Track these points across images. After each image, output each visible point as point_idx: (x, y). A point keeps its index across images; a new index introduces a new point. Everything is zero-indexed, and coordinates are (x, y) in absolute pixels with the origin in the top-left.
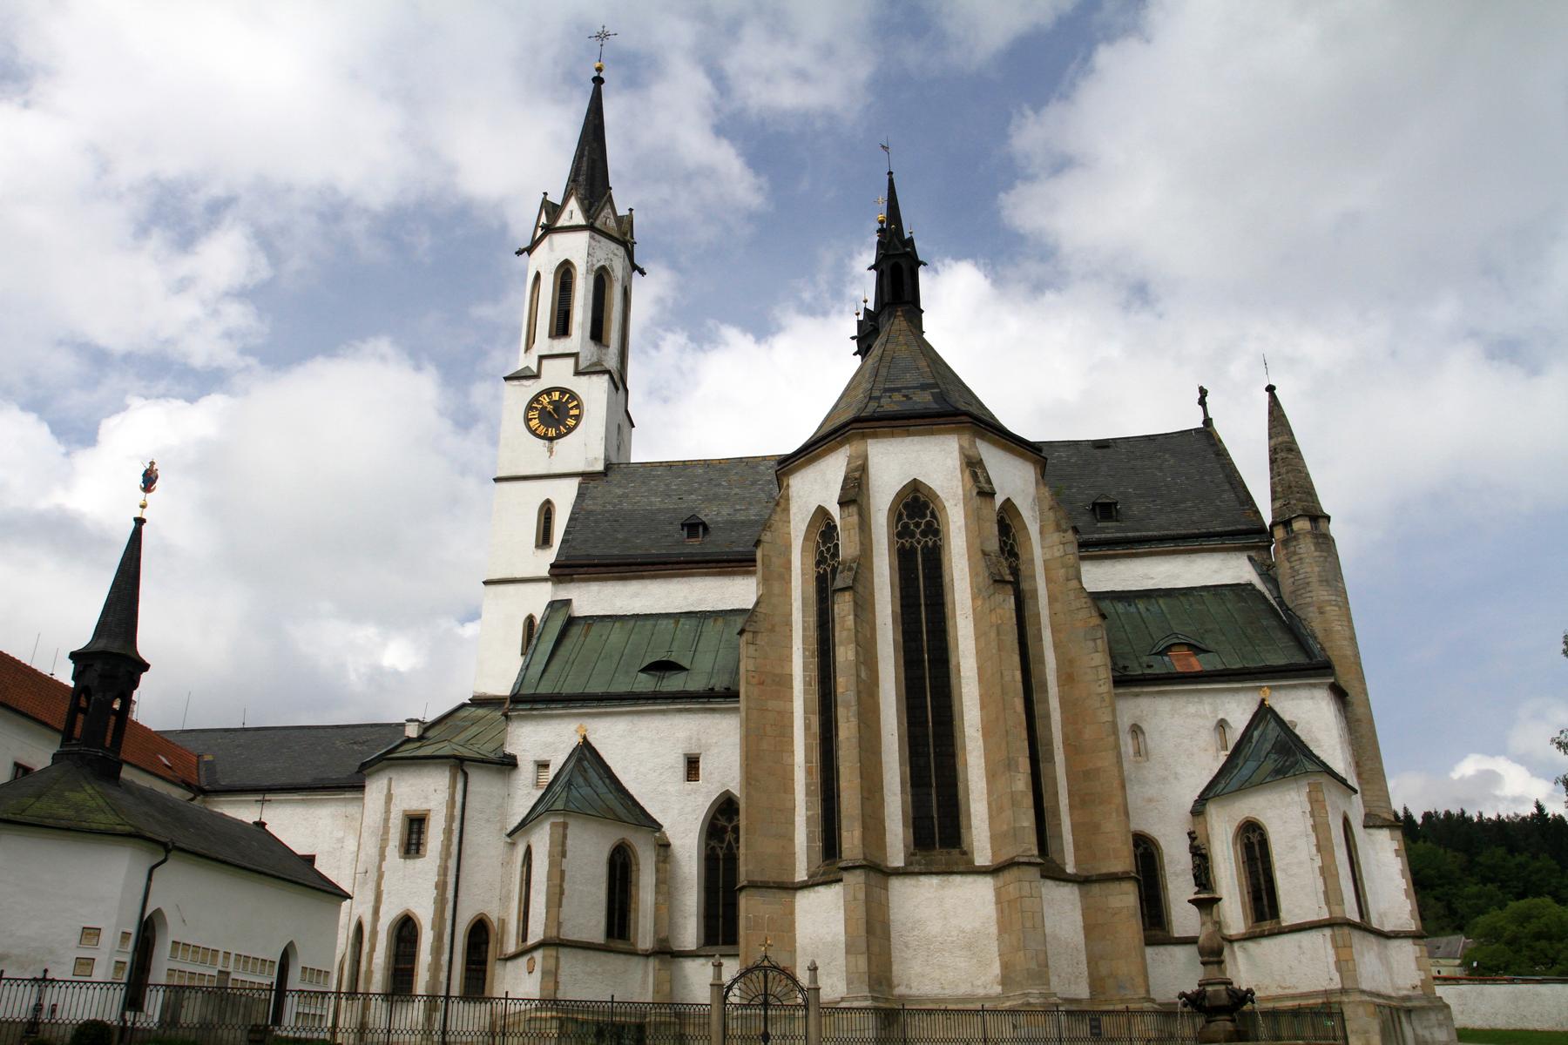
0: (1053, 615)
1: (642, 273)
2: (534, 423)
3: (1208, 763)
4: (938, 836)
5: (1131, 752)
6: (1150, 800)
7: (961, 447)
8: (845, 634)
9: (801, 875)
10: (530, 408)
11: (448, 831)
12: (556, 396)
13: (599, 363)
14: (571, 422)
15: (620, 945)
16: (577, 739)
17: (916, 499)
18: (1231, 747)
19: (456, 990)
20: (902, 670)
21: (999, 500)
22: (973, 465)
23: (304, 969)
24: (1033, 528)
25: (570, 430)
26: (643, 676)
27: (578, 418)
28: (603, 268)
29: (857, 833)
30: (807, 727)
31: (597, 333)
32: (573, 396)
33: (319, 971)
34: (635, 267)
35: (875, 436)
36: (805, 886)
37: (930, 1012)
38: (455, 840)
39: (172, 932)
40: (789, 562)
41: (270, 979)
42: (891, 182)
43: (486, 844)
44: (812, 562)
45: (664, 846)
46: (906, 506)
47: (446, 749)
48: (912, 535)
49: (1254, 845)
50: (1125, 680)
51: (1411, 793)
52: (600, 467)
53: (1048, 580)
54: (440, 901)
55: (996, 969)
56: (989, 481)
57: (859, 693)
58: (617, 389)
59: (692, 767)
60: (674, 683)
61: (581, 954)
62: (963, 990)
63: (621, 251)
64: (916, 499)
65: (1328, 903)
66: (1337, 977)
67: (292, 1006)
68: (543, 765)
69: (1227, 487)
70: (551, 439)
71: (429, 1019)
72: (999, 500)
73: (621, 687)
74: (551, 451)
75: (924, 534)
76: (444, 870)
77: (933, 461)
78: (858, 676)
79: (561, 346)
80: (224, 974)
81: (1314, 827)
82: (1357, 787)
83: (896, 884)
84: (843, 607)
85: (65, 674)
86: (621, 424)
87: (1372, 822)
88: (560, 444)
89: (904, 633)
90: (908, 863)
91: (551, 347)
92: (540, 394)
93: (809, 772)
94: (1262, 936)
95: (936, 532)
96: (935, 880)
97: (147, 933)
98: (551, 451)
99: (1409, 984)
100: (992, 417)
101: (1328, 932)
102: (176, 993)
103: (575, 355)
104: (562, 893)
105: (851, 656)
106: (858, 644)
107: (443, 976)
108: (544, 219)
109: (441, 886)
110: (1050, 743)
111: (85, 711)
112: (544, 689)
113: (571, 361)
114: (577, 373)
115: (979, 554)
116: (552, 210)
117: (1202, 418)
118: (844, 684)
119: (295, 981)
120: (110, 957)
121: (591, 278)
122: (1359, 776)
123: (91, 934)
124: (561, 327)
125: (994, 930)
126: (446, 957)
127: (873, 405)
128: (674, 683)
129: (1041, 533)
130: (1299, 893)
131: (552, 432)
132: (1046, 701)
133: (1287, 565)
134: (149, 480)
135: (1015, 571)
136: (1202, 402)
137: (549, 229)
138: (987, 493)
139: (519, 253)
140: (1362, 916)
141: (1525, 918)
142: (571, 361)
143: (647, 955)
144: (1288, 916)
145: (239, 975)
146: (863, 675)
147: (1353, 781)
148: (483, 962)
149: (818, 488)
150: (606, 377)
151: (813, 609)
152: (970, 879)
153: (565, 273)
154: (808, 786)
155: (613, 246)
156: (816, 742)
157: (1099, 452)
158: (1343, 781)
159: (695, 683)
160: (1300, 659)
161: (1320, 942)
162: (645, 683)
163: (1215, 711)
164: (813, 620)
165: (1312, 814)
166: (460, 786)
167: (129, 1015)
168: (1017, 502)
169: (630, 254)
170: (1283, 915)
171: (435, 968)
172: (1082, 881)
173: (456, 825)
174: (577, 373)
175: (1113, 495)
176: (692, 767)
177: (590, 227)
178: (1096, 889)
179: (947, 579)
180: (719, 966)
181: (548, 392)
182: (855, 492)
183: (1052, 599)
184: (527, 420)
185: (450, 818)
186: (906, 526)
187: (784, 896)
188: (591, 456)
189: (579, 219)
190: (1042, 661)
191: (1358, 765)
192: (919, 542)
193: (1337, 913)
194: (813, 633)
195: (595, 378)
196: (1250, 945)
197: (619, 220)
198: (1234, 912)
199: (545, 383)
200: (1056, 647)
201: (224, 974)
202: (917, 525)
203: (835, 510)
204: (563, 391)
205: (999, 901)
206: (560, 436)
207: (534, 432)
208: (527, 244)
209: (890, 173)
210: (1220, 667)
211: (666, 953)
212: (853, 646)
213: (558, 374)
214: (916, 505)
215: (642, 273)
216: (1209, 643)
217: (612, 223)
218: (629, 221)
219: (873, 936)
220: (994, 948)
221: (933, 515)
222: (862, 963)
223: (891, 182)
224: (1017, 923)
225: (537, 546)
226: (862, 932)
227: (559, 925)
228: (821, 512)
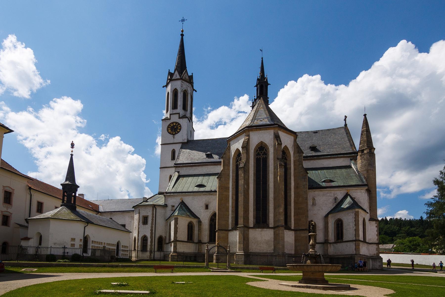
0: (295, 173)
1: (196, 91)
2: (170, 131)
3: (330, 206)
4: (261, 221)
5: (311, 203)
6: (315, 214)
7: (274, 133)
8: (241, 178)
9: (230, 228)
10: (168, 127)
11: (152, 220)
12: (175, 124)
13: (185, 115)
14: (178, 130)
15: (190, 241)
16: (181, 201)
17: (261, 146)
18: (337, 203)
19: (156, 250)
20: (255, 186)
21: (283, 146)
22: (277, 137)
23: (122, 246)
24: (292, 153)
25: (178, 132)
26: (196, 188)
27: (180, 129)
28: (185, 90)
29: (242, 220)
30: (232, 198)
31: (185, 108)
32: (179, 124)
33: (113, 244)
34: (194, 90)
35: (252, 131)
36: (230, 230)
37: (257, 255)
38: (154, 221)
39: (92, 238)
40: (230, 162)
41: (116, 248)
42: (262, 60)
43: (160, 221)
44: (235, 161)
45: (200, 222)
46: (259, 148)
47: (151, 203)
48: (260, 155)
49: (339, 225)
50: (309, 189)
51: (381, 213)
52: (186, 141)
53: (294, 165)
54: (152, 233)
55: (273, 247)
56: (280, 141)
57: (244, 191)
58: (190, 122)
59: (207, 207)
60: (202, 189)
61: (182, 243)
62: (265, 251)
63: (190, 86)
64: (261, 146)
65: (355, 236)
66: (355, 252)
67: (121, 253)
68: (173, 206)
69: (348, 141)
70: (174, 135)
71: (151, 255)
72: (283, 146)
73: (190, 190)
74: (174, 137)
75: (263, 155)
76: (152, 227)
77: (267, 137)
78: (244, 187)
79: (175, 111)
80: (104, 247)
81: (355, 221)
82: (369, 212)
83: (251, 230)
84: (241, 174)
85: (60, 187)
86: (192, 131)
87: (371, 219)
88: (176, 136)
89: (256, 177)
90: (254, 226)
91: (173, 112)
92: (171, 124)
93: (232, 207)
94: (338, 243)
95: (266, 154)
96: (260, 230)
97: (86, 240)
98: (174, 137)
99: (373, 253)
100: (284, 125)
101: (354, 242)
102: (94, 251)
103: (179, 114)
104: (177, 231)
105: (243, 183)
106: (244, 180)
107: (153, 247)
108: (169, 78)
109: (152, 230)
110: (291, 202)
111: (66, 196)
112: (173, 191)
113: (178, 115)
114: (179, 118)
115: (276, 159)
116: (171, 74)
117: (344, 124)
118: (241, 189)
119: (121, 248)
120: (78, 243)
121: (182, 93)
122: (370, 210)
123: (73, 239)
124: (175, 106)
125: (273, 240)
126: (153, 243)
127: (251, 124)
128: (202, 189)
129: (294, 154)
130: (349, 234)
131: (174, 133)
132: (291, 193)
133: (360, 161)
134: (73, 145)
135: (286, 164)
136: (345, 120)
137: (171, 80)
138: (280, 144)
139: (164, 87)
140: (364, 239)
141: (410, 242)
142: (178, 115)
143: (196, 243)
144: (345, 238)
145: (107, 247)
146: (245, 187)
147: (368, 211)
148: (162, 245)
149: (237, 145)
150: (187, 119)
151: (235, 172)
152: (268, 230)
153: (175, 93)
154: (232, 210)
155: (188, 84)
156: (234, 201)
157: (314, 134)
158: (365, 211)
159: (207, 189)
160: (360, 183)
161: (352, 245)
162: (196, 189)
163: (334, 195)
164: (234, 175)
165: (355, 218)
166: (155, 211)
167: (85, 255)
168: (288, 146)
169: (193, 86)
170: (344, 239)
171: (151, 245)
172: (295, 230)
173: (154, 219)
174: (179, 118)
175: (316, 144)
176: (207, 207)
177: (181, 79)
178: (298, 232)
179: (268, 165)
180: (207, 246)
181: (173, 123)
182: (246, 146)
183: (295, 169)
184: (168, 130)
185: (153, 217)
186: (258, 153)
187: (226, 232)
188: (184, 139)
189: (178, 77)
190: (291, 184)
191: (370, 207)
192: (262, 156)
193: (357, 238)
194: (235, 178)
195: (184, 119)
196: (335, 245)
197: (189, 77)
198: (332, 237)
199: (172, 121)
200: (294, 180)
201: (104, 247)
202: (261, 153)
203: (241, 149)
204: (176, 123)
205: (274, 234)
206: (176, 134)
207: (170, 133)
208: (166, 84)
209: (262, 58)
210: (337, 185)
211: (200, 242)
212: (243, 180)
213: (175, 119)
214: (262, 149)
215: (196, 91)
216: (335, 180)
217: (187, 78)
218: (191, 77)
219: (245, 240)
220: (273, 243)
221: (266, 150)
222: (242, 245)
223: (262, 60)
224: (277, 239)
225: (172, 160)
226: (242, 240)
227: (177, 238)
228: (238, 150)
